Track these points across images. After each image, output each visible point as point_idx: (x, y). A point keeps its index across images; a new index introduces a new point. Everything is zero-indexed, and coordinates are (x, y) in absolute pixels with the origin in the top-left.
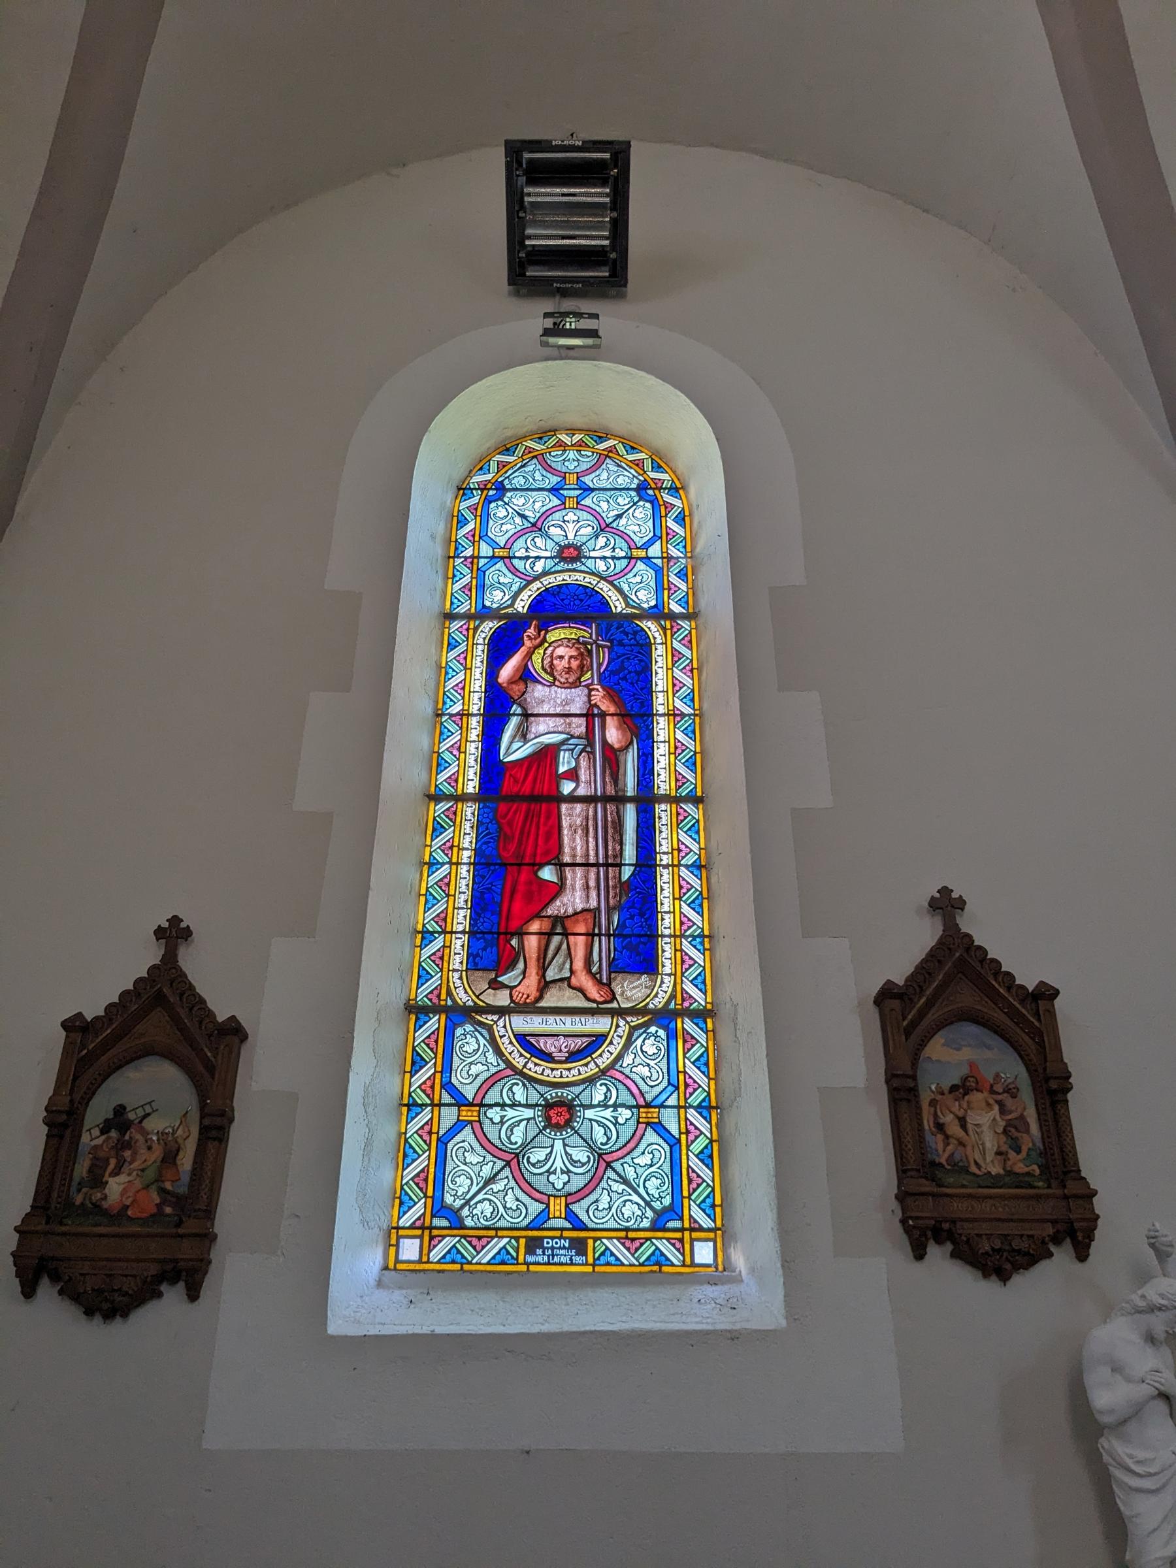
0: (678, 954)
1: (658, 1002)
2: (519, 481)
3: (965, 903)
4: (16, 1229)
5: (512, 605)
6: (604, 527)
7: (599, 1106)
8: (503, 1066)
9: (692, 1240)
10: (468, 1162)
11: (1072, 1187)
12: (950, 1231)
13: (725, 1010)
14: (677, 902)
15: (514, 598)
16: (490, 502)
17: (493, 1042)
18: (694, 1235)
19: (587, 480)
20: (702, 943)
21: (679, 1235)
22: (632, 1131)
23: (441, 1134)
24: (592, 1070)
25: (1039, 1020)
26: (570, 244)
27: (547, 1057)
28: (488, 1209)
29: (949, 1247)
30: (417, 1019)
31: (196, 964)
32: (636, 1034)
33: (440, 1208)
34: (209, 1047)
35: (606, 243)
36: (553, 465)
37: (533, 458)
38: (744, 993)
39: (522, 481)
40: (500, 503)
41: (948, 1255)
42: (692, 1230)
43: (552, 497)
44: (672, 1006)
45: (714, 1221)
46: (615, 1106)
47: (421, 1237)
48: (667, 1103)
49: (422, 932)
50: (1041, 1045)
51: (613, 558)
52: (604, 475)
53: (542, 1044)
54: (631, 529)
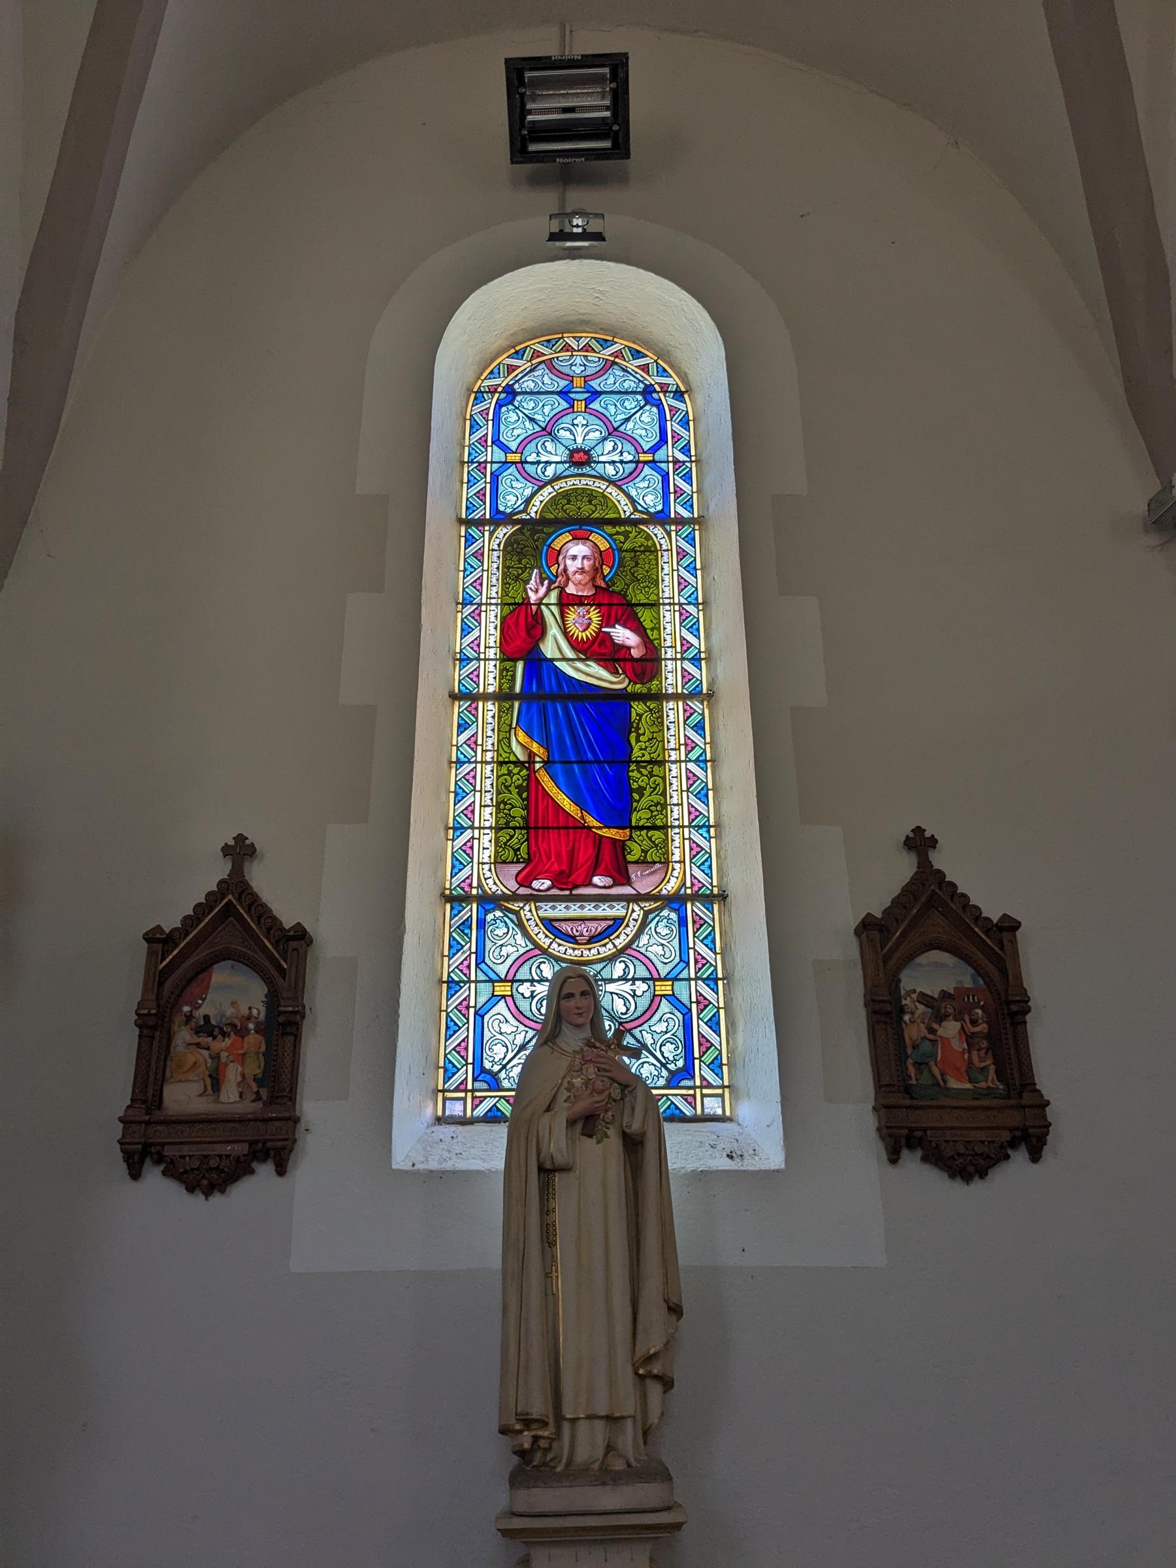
0: (687, 842)
1: (671, 886)
2: (528, 385)
3: (936, 841)
4: (121, 1120)
5: (525, 511)
6: (613, 431)
7: (619, 979)
8: (531, 946)
9: (703, 1096)
10: (644, 426)
11: (1027, 1099)
12: (921, 1139)
13: (731, 891)
14: (685, 794)
15: (528, 501)
16: (501, 406)
17: (521, 925)
18: (705, 1091)
19: (594, 384)
20: (708, 832)
21: (691, 1092)
22: (647, 1006)
23: (478, 1006)
24: (608, 950)
25: (1002, 948)
26: (571, 145)
27: (572, 939)
28: (627, 404)
29: (919, 1153)
30: (452, 908)
31: (263, 879)
32: (651, 916)
33: (481, 1072)
34: (281, 953)
35: (607, 114)
36: (560, 369)
37: (540, 363)
38: (747, 880)
39: (532, 385)
40: (511, 407)
41: (918, 1160)
42: (701, 1087)
43: (561, 401)
44: (682, 891)
45: (722, 1079)
46: (634, 980)
47: (464, 1099)
48: (681, 976)
49: (448, 982)
50: (1004, 972)
51: (622, 462)
52: (611, 380)
53: (566, 927)
54: (638, 433)
